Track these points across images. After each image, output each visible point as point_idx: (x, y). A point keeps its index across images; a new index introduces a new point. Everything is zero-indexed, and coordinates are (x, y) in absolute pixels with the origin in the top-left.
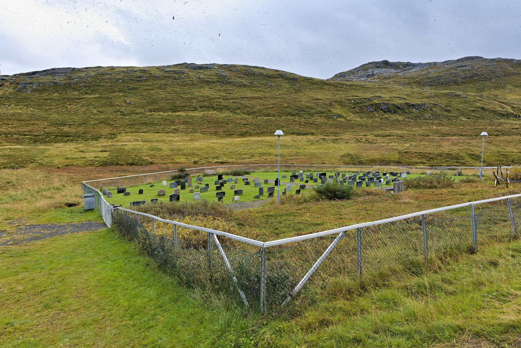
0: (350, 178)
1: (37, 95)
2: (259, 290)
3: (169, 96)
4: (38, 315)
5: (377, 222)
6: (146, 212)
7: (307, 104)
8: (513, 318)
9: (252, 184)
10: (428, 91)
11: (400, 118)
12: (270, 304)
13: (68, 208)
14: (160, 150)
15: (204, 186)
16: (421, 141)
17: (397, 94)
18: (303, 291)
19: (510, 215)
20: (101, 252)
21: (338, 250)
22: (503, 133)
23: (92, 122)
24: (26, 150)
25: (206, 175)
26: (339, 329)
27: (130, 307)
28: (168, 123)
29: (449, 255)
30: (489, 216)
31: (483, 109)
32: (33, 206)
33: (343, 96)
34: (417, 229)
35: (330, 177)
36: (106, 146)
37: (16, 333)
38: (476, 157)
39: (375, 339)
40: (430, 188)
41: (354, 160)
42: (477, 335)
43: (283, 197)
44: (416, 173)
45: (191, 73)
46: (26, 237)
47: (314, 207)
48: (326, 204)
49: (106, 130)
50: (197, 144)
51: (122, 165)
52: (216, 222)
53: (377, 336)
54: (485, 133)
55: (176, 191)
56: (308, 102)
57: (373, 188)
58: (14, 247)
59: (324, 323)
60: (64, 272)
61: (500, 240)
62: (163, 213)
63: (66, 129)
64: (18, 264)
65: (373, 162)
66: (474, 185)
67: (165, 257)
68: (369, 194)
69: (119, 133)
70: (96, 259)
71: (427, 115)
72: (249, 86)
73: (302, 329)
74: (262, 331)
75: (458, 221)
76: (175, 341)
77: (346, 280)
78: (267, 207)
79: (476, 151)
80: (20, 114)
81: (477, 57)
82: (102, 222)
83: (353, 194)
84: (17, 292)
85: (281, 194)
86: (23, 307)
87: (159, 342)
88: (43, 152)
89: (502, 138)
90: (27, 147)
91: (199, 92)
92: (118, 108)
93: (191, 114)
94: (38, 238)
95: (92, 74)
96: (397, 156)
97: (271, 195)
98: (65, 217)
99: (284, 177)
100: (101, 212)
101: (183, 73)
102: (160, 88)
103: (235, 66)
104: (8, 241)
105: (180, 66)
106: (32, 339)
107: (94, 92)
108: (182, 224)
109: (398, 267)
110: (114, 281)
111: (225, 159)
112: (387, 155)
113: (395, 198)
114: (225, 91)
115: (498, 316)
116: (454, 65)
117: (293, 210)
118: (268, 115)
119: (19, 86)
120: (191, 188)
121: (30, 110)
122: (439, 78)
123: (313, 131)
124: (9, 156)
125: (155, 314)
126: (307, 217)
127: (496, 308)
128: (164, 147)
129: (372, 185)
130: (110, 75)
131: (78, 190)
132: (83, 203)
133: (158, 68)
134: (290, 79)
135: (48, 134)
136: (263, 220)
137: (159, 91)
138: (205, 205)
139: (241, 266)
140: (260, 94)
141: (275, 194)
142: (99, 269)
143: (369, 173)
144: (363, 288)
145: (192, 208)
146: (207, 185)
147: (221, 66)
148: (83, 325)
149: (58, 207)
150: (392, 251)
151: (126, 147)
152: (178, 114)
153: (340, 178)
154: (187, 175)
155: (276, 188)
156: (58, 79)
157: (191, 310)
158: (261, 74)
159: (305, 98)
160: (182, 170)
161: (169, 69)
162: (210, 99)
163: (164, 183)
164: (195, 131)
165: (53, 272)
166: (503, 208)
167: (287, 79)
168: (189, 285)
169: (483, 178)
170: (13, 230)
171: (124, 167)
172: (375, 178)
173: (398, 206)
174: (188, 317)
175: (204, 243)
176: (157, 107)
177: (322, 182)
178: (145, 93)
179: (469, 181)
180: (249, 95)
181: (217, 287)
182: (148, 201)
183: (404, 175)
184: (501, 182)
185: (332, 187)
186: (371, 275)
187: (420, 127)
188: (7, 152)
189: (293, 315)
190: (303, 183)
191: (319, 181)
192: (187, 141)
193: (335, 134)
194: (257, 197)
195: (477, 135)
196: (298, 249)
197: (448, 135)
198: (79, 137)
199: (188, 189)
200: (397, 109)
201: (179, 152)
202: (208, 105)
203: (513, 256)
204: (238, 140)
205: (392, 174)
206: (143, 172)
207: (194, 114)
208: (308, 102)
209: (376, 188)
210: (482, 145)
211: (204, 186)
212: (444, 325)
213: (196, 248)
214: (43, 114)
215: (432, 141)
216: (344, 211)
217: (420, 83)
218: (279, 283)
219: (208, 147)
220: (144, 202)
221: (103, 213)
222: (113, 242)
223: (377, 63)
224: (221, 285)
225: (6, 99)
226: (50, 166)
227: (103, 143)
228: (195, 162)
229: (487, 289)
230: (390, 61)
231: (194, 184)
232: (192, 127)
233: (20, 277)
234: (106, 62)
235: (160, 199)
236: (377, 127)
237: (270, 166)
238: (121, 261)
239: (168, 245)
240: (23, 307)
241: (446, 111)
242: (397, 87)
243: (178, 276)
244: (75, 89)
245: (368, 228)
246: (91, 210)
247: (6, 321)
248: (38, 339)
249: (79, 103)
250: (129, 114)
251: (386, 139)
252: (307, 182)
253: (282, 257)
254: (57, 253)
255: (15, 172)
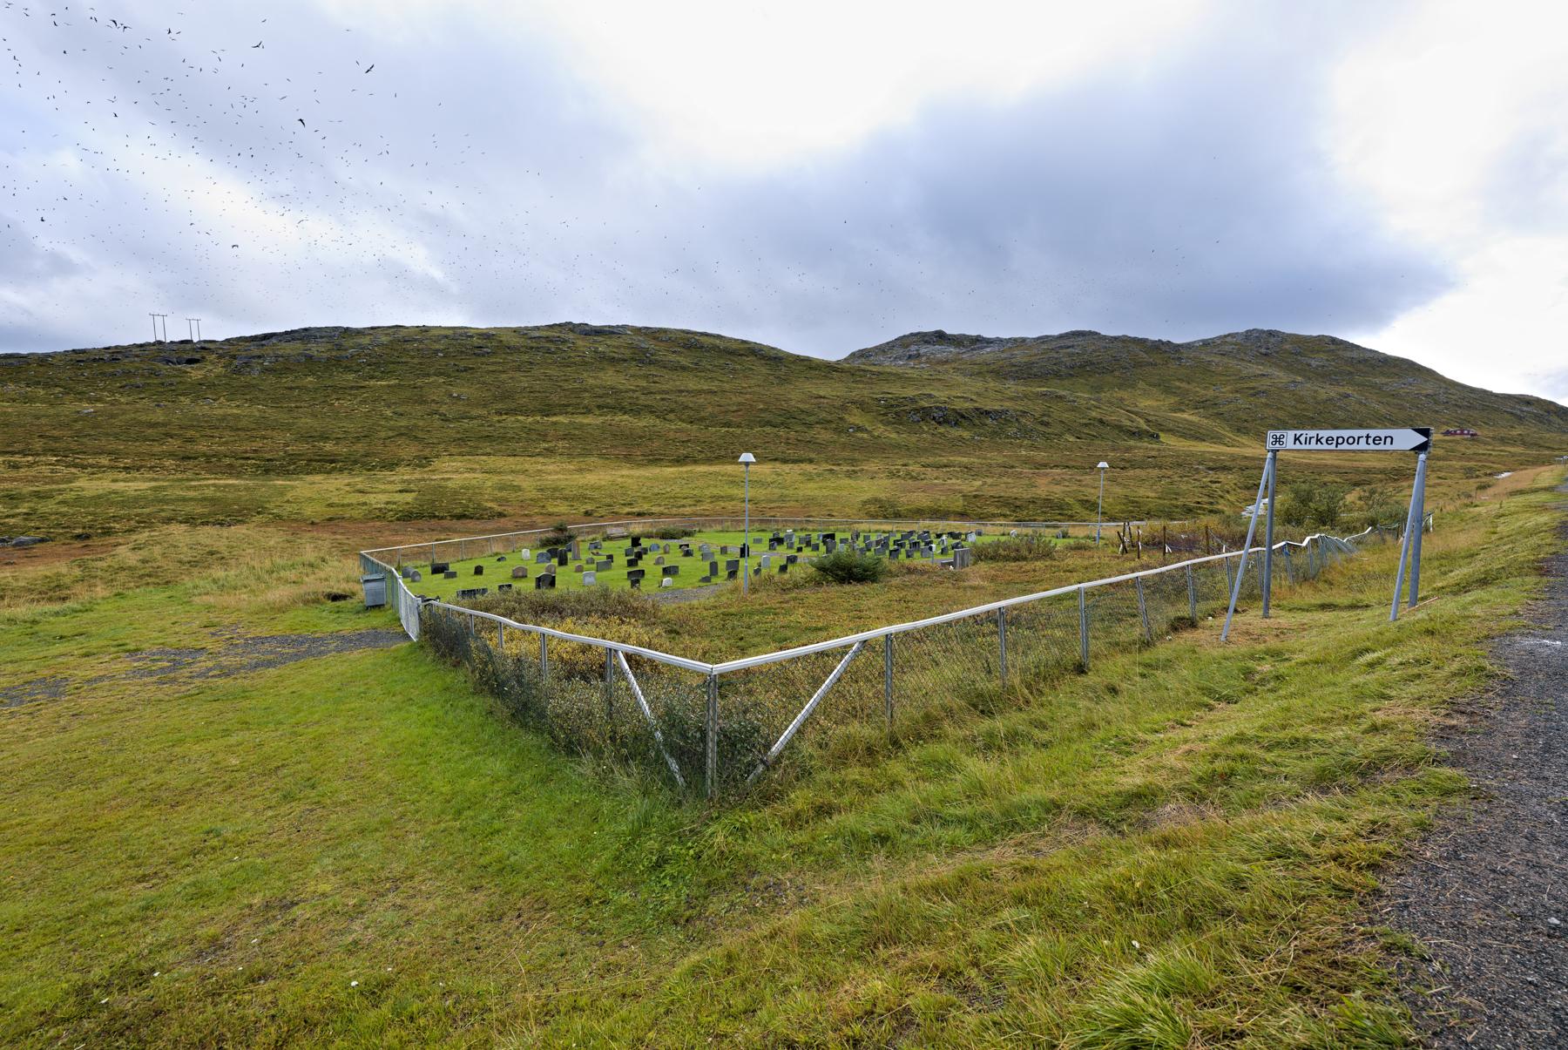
0: (878, 543)
1: (272, 379)
2: (704, 754)
3: (537, 385)
4: (270, 813)
5: (921, 623)
6: (487, 610)
7: (801, 406)
8: (1138, 781)
9: (697, 555)
10: (1012, 387)
11: (966, 434)
12: (729, 781)
13: (330, 604)
14: (519, 488)
15: (604, 559)
16: (1001, 476)
17: (960, 391)
18: (787, 753)
19: (1142, 606)
20: (398, 688)
21: (852, 675)
22: (1133, 465)
23: (383, 435)
24: (247, 489)
25: (609, 538)
26: (849, 820)
27: (455, 794)
28: (534, 437)
29: (1043, 678)
30: (1108, 608)
31: (1101, 421)
32: (260, 600)
33: (865, 392)
34: (992, 633)
35: (842, 541)
36: (409, 482)
37: (226, 850)
38: (1090, 506)
39: (913, 833)
40: (1016, 559)
41: (885, 510)
42: (1083, 813)
43: (755, 579)
44: (992, 533)
45: (580, 343)
46: (245, 661)
47: (812, 596)
48: (834, 591)
49: (409, 450)
50: (591, 478)
52: (624, 627)
53: (917, 827)
54: (1105, 465)
55: (548, 569)
56: (801, 401)
57: (918, 560)
58: (221, 681)
59: (824, 811)
60: (323, 730)
61: (1125, 649)
62: (522, 611)
63: (329, 447)
64: (230, 715)
65: (919, 513)
66: (1087, 553)
67: (523, 698)
68: (910, 571)
69: (437, 456)
70: (387, 702)
71: (1011, 431)
72: (693, 370)
73: (784, 824)
74: (710, 831)
75: (1060, 618)
76: (543, 856)
77: (859, 730)
78: (724, 599)
79: (1091, 494)
80: (237, 417)
81: (1090, 333)
82: (399, 630)
83: (882, 573)
84: (226, 770)
85: (751, 572)
86: (240, 799)
87: (512, 859)
88: (282, 492)
89: (1131, 473)
90: (250, 483)
91: (595, 378)
93: (580, 419)
94: (270, 664)
95: (384, 339)
96: (961, 502)
97: (732, 575)
98: (326, 622)
99: (758, 541)
100: (398, 611)
101: (564, 342)
102: (518, 369)
103: (665, 331)
104: (210, 669)
106: (259, 860)
107: (386, 374)
108: (558, 632)
109: (957, 703)
110: (423, 745)
111: (645, 507)
112: (944, 502)
113: (957, 579)
114: (646, 377)
115: (1117, 779)
116: (1054, 344)
117: (773, 603)
118: (728, 424)
119: (236, 362)
120: (578, 563)
121: (257, 410)
122: (1029, 365)
123: (813, 455)
124: (213, 501)
125: (505, 808)
126: (798, 616)
127: (1114, 766)
128: (526, 483)
129: (917, 555)
130: (421, 342)
131: (353, 567)
132: (362, 593)
133: (515, 330)
134: (770, 359)
135: (293, 458)
136: (717, 623)
137: (518, 374)
138: (605, 594)
139: (669, 710)
140: (714, 386)
141: (740, 574)
142: (383, 726)
143: (911, 533)
144: (895, 743)
145: (579, 601)
146: (610, 557)
147: (638, 330)
148: (362, 831)
149: (312, 601)
150: (947, 673)
151: (450, 484)
152: (554, 419)
153: (860, 543)
154: (571, 538)
155: (742, 562)
156: (314, 349)
157: (575, 798)
158: (715, 348)
159: (797, 394)
160: (561, 529)
161: (537, 334)
162: (616, 391)
163: (526, 553)
164: (586, 453)
165: (300, 729)
166: (1131, 593)
167: (763, 357)
168: (571, 749)
169: (1101, 543)
170: (220, 647)
171: (445, 523)
172: (921, 544)
173: (960, 592)
174: (569, 811)
175: (599, 670)
176: (513, 406)
177: (828, 551)
178: (489, 379)
179: (1079, 548)
180: (692, 385)
181: (624, 751)
182: (493, 588)
183: (973, 538)
184: (1130, 548)
185: (845, 560)
186: (911, 719)
187: (1000, 451)
188: (209, 492)
189: (768, 798)
190: (792, 552)
191: (823, 548)
192: (571, 472)
193: (853, 462)
194: (706, 579)
195: (1093, 467)
196: (780, 676)
197: (1045, 466)
198: (355, 462)
199: (572, 565)
200: (958, 418)
201: (556, 493)
202: (614, 403)
203: (1143, 676)
204: (670, 471)
205: (951, 535)
206: (483, 532)
207: (586, 421)
208: (801, 401)
209: (924, 561)
210: (1100, 487)
211: (604, 559)
212: (1029, 801)
213: (585, 678)
214: (283, 417)
215: (1019, 476)
216: (865, 604)
217: (999, 373)
218: (743, 741)
219: (613, 483)
220: (484, 591)
221: (403, 613)
222: (422, 670)
223: (925, 334)
224: (633, 748)
225: (209, 387)
226: (296, 520)
227: (404, 474)
228: (587, 514)
229: (1101, 734)
230: (948, 332)
231: (585, 555)
232: (581, 445)
233: (232, 740)
234: (411, 318)
235: (516, 585)
236: (926, 450)
237: (732, 520)
238: (437, 707)
239: (529, 674)
240: (240, 799)
241: (1042, 423)
242: (961, 379)
243: (550, 733)
244: (348, 369)
245: (906, 633)
246: (378, 607)
247: (206, 827)
248: (270, 860)
249: (356, 396)
250: (457, 419)
251: (941, 473)
252: (800, 550)
253: (750, 692)
254: (308, 692)
255: (225, 532)
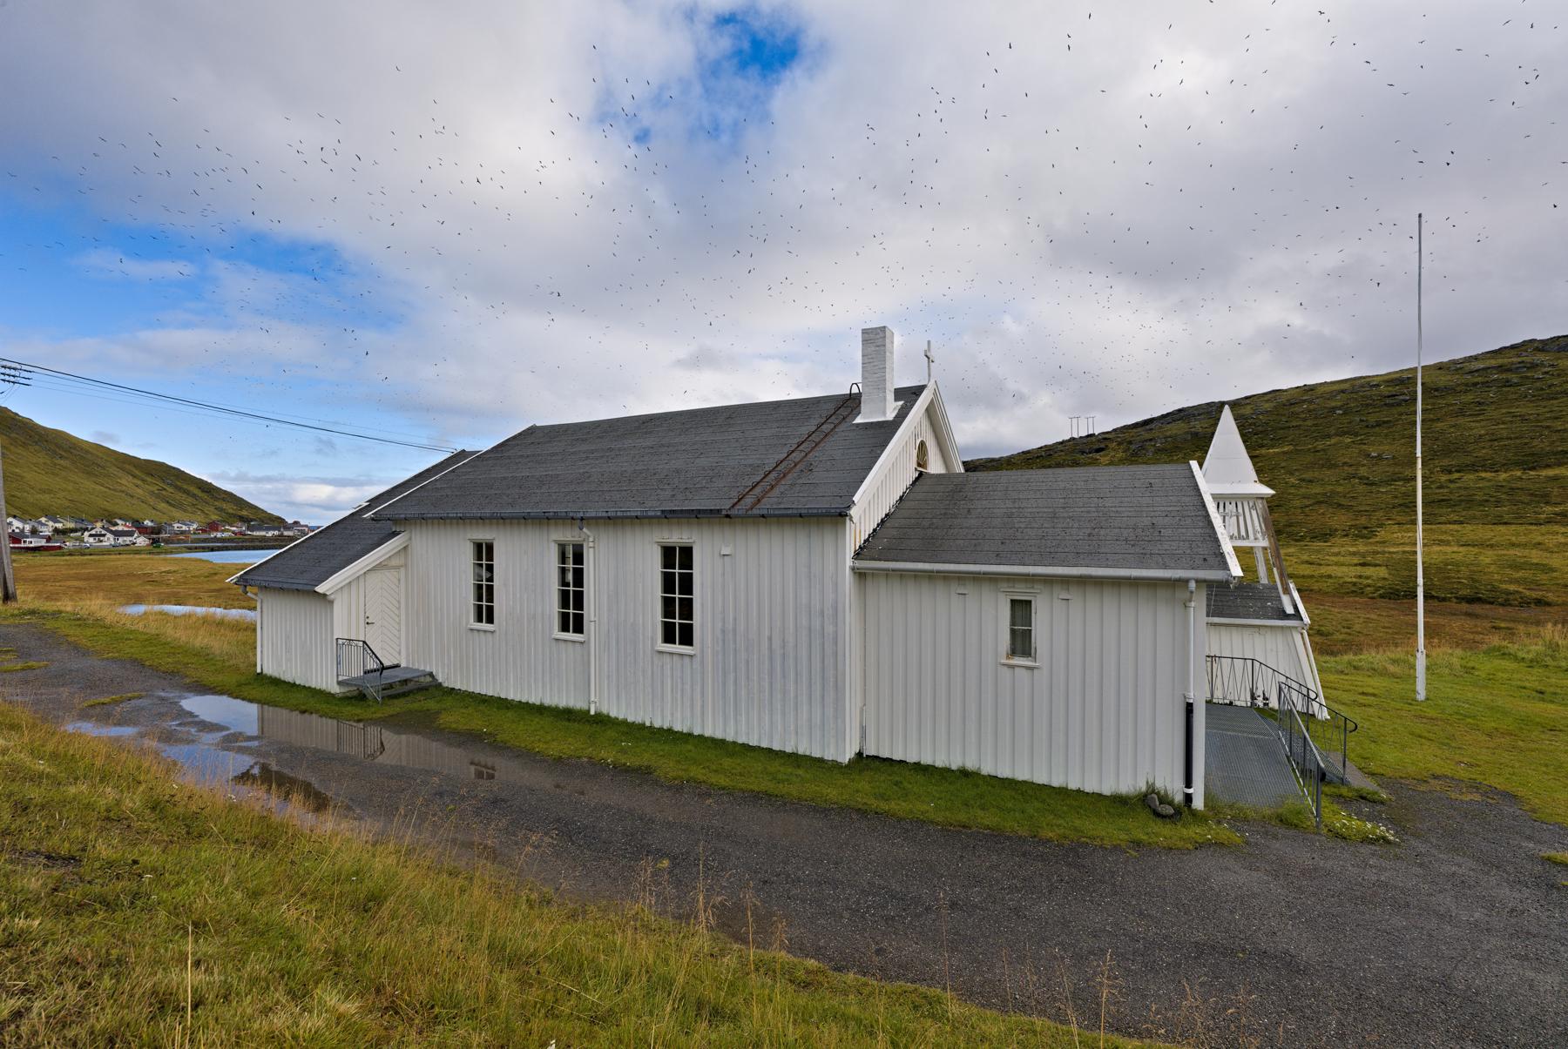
23: (1297, 503)
28: (1526, 499)
51: (1444, 599)
69: (1381, 526)
92: (1351, 470)
95: (1267, 406)
101: (1533, 366)
105: (1513, 352)
107: (1276, 442)
119: (1133, 447)
176: (1469, 460)
